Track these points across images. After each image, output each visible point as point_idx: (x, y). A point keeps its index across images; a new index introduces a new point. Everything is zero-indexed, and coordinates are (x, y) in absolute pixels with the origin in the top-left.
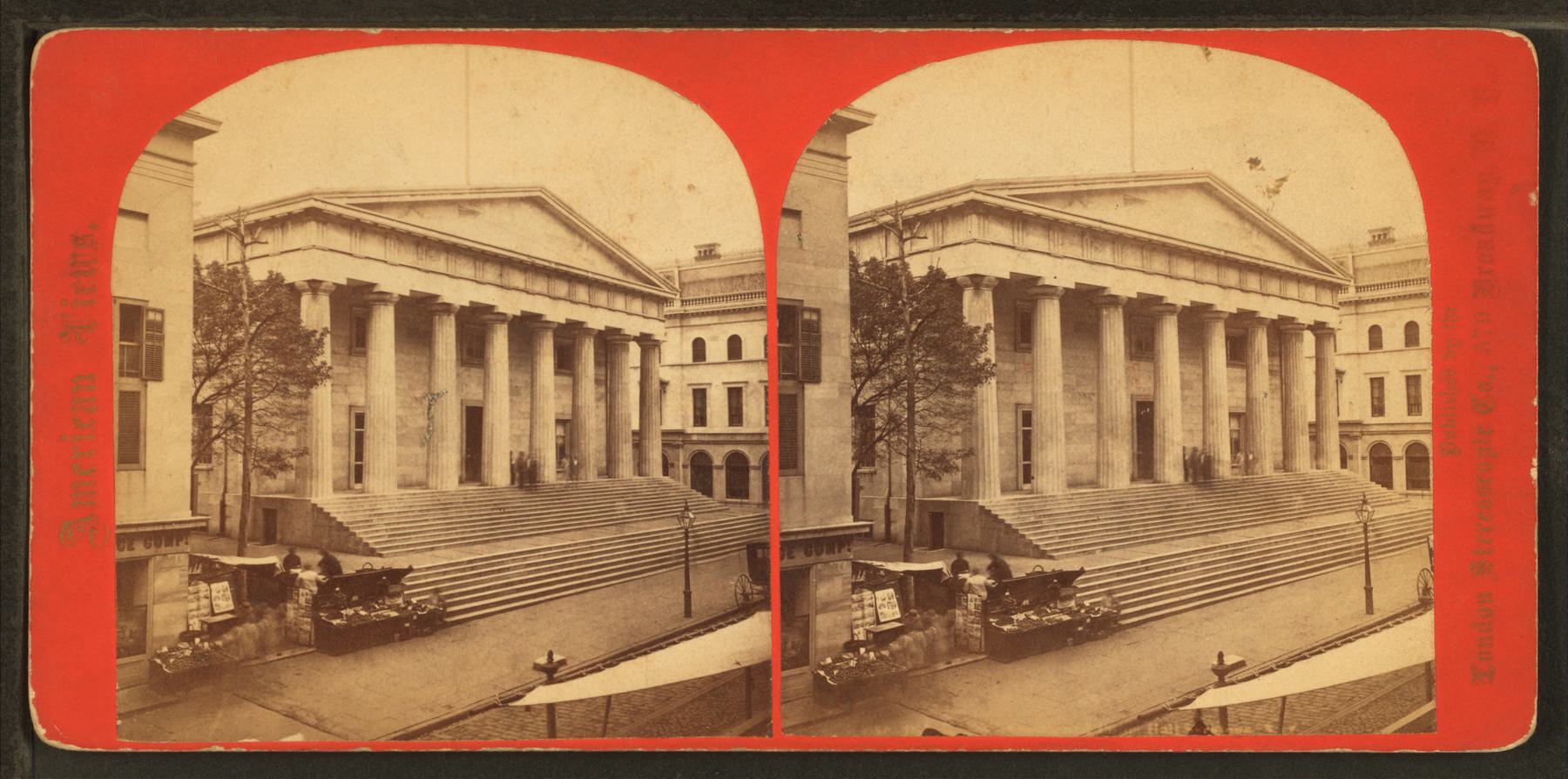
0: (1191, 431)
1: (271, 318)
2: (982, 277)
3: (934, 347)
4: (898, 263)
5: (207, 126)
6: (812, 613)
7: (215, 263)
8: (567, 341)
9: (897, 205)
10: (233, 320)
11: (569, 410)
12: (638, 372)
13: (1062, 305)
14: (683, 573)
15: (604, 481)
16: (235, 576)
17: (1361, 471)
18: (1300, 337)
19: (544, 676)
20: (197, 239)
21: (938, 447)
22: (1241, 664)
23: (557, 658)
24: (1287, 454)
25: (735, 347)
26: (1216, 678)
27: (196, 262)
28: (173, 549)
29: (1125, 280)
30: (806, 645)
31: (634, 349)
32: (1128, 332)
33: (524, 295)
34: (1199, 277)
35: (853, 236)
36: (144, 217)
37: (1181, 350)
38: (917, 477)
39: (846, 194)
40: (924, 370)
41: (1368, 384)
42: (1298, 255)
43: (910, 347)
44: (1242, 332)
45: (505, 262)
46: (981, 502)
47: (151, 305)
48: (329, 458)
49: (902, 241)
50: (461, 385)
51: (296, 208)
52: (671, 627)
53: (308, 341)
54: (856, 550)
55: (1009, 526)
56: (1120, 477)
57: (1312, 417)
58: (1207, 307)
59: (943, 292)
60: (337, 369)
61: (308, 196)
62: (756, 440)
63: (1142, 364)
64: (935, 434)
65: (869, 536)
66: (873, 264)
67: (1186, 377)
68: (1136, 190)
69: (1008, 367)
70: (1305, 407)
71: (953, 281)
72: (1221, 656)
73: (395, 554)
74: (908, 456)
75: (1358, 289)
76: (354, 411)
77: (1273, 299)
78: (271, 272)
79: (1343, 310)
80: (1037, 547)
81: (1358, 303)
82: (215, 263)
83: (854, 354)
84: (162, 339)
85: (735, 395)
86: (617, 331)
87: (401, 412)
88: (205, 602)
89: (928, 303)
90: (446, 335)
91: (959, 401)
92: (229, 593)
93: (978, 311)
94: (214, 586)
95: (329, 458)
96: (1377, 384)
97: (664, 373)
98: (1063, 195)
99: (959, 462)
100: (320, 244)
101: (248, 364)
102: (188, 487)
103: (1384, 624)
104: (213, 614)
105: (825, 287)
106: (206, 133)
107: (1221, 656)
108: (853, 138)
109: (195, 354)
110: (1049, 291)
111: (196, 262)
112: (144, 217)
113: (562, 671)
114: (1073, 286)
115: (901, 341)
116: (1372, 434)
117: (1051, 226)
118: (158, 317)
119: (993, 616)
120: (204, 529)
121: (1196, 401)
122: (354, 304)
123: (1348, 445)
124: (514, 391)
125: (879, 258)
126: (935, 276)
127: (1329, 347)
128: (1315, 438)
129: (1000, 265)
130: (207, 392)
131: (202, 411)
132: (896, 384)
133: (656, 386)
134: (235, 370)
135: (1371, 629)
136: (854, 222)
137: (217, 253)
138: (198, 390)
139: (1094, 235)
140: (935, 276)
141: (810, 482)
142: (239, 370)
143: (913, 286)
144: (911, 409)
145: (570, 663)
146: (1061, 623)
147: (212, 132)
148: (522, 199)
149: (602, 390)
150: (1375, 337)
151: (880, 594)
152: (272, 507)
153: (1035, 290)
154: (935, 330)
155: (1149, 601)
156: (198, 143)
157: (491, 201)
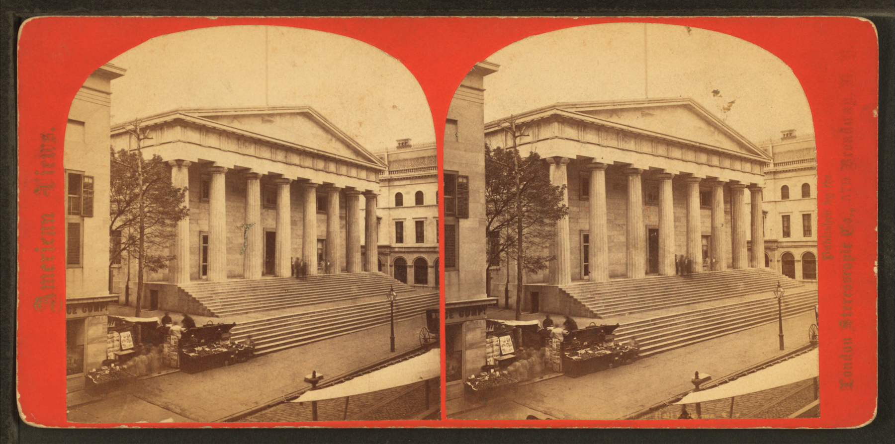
0: (680, 246)
1: (155, 181)
2: (561, 158)
3: (533, 198)
4: (513, 150)
5: (118, 72)
6: (463, 349)
7: (123, 150)
8: (324, 195)
9: (512, 117)
10: (133, 182)
11: (325, 234)
12: (364, 212)
13: (606, 174)
14: (390, 326)
15: (730, 271)
16: (134, 328)
17: (777, 268)
18: (742, 192)
19: (311, 385)
20: (112, 136)
21: (536, 255)
22: (709, 379)
23: (318, 375)
24: (735, 259)
25: (419, 198)
26: (694, 387)
27: (112, 149)
28: (99, 313)
29: (642, 159)
30: (460, 367)
31: (362, 199)
32: (644, 189)
33: (299, 168)
34: (684, 158)
35: (487, 135)
36: (82, 124)
37: (674, 199)
38: (523, 272)
39: (483, 110)
40: (527, 211)
41: (781, 219)
42: (741, 145)
43: (520, 198)
44: (709, 189)
45: (288, 149)
46: (560, 286)
47: (86, 174)
48: (188, 261)
49: (515, 137)
50: (263, 219)
51: (169, 119)
52: (770, 357)
53: (176, 195)
54: (489, 313)
55: (576, 300)
56: (640, 272)
57: (749, 238)
58: (689, 175)
59: (538, 166)
60: (192, 211)
61: (176, 112)
62: (432, 251)
63: (652, 207)
64: (534, 248)
65: (496, 305)
66: (498, 150)
67: (677, 215)
68: (649, 108)
69: (575, 209)
70: (745, 232)
71: (544, 160)
72: (697, 374)
73: (226, 316)
74: (518, 260)
75: (775, 165)
76: (202, 234)
77: (726, 171)
78: (154, 155)
79: (767, 177)
80: (592, 312)
81: (775, 173)
82: (123, 150)
83: (488, 202)
84: (92, 193)
85: (420, 225)
86: (352, 189)
87: (229, 235)
88: (117, 343)
89: (530, 173)
90: (255, 191)
91: (547, 229)
92: (130, 338)
93: (558, 177)
94: (122, 334)
95: (188, 261)
96: (786, 219)
97: (379, 213)
98: (606, 111)
99: (547, 263)
100: (182, 139)
101: (141, 208)
102: (107, 278)
103: (790, 356)
104: (122, 350)
105: (471, 164)
106: (118, 76)
107: (697, 374)
108: (487, 79)
109: (112, 202)
110: (599, 166)
111: (112, 149)
112: (82, 124)
113: (321, 382)
114: (612, 163)
115: (514, 195)
116: (783, 247)
117: (600, 129)
118: (90, 181)
119: (567, 351)
120: (117, 302)
121: (683, 229)
122: (202, 173)
123: (770, 253)
124: (293, 223)
125: (502, 147)
126: (534, 157)
127: (759, 197)
128: (750, 250)
129: (571, 151)
130: (118, 223)
131: (115, 234)
132: (512, 219)
133: (374, 220)
134: (134, 211)
135: (782, 359)
136: (488, 126)
137: (124, 144)
138: (113, 222)
139: (624, 134)
140: (534, 157)
141: (462, 275)
142: (136, 211)
143: (521, 163)
144: (520, 233)
145: (325, 378)
146: (606, 355)
147: (121, 75)
148: (298, 114)
149: (344, 222)
150: (785, 192)
151: (502, 338)
152: (155, 289)
153: (591, 165)
154: (533, 188)
155: (656, 343)
156: (113, 82)
157: (280, 115)
